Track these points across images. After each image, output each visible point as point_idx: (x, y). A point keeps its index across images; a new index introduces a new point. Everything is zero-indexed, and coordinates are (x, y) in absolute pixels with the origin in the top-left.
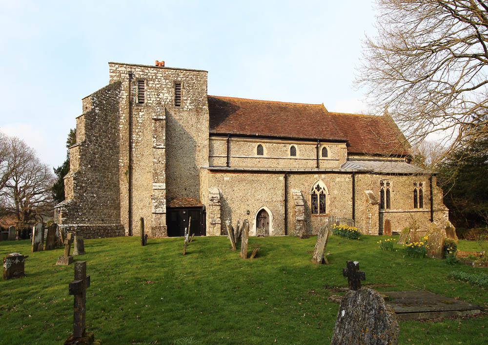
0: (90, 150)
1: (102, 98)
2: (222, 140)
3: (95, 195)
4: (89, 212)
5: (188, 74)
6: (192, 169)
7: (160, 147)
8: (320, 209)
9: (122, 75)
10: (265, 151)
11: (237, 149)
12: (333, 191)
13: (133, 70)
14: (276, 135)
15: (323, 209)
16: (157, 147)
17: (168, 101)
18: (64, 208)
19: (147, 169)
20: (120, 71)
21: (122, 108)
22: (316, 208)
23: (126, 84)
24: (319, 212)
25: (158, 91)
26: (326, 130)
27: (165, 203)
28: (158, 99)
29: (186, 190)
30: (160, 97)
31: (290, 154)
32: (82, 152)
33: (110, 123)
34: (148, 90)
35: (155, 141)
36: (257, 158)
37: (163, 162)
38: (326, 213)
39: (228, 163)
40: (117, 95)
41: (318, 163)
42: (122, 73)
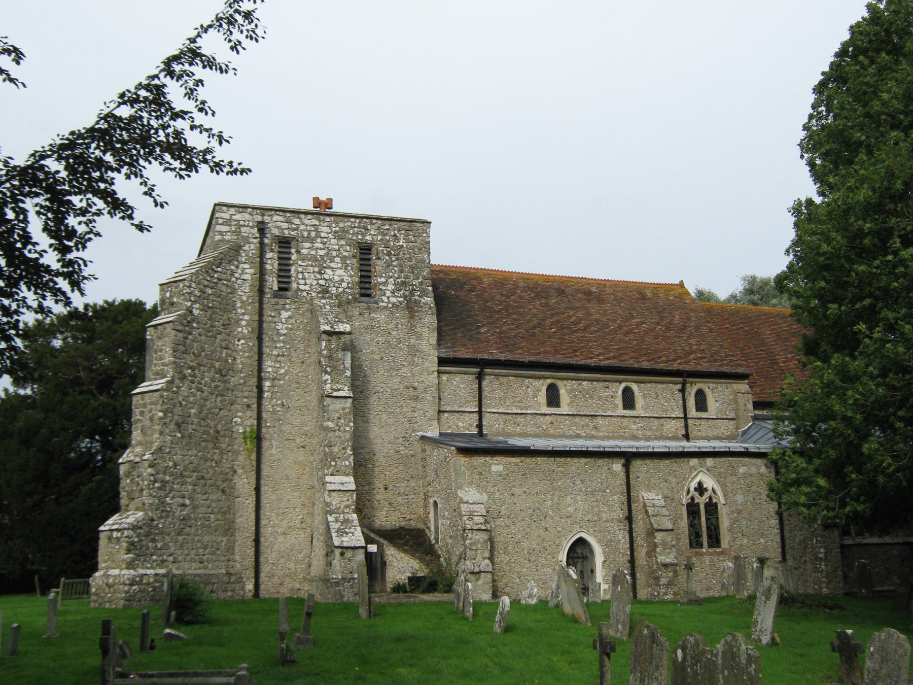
2: (466, 373)
3: (187, 502)
4: (176, 542)
5: (387, 227)
8: (709, 537)
9: (243, 229)
11: (498, 394)
12: (734, 495)
13: (267, 219)
14: (588, 362)
15: (715, 540)
16: (335, 394)
17: (344, 285)
18: (131, 533)
19: (298, 440)
20: (239, 221)
21: (243, 302)
22: (698, 535)
23: (252, 248)
24: (705, 544)
25: (321, 265)
26: (697, 349)
27: (356, 522)
28: (322, 282)
29: (386, 489)
30: (326, 276)
31: (621, 405)
32: (167, 403)
34: (300, 262)
35: (329, 381)
36: (546, 415)
37: (348, 429)
38: (723, 546)
39: (480, 426)
40: (233, 273)
42: (244, 226)
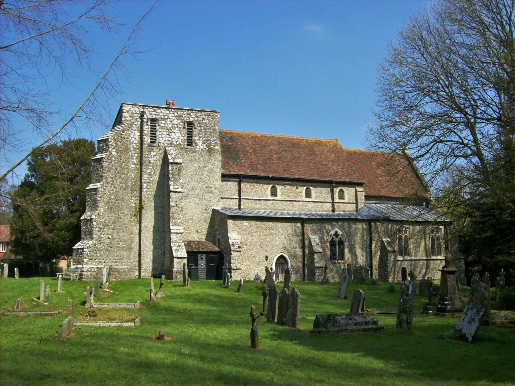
0: (107, 192)
1: (118, 140)
3: (110, 237)
5: (200, 114)
6: (204, 211)
7: (177, 190)
9: (135, 115)
10: (313, 194)
13: (146, 110)
17: (180, 140)
21: (134, 148)
29: (197, 232)
33: (123, 164)
39: (239, 205)
41: (333, 206)
